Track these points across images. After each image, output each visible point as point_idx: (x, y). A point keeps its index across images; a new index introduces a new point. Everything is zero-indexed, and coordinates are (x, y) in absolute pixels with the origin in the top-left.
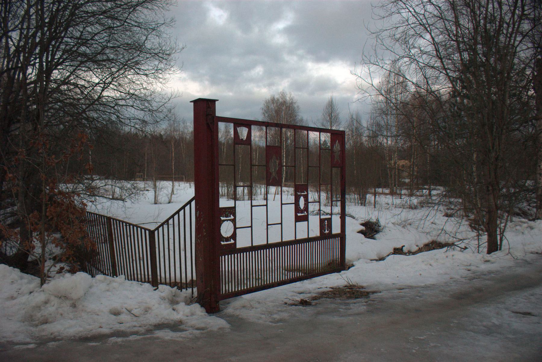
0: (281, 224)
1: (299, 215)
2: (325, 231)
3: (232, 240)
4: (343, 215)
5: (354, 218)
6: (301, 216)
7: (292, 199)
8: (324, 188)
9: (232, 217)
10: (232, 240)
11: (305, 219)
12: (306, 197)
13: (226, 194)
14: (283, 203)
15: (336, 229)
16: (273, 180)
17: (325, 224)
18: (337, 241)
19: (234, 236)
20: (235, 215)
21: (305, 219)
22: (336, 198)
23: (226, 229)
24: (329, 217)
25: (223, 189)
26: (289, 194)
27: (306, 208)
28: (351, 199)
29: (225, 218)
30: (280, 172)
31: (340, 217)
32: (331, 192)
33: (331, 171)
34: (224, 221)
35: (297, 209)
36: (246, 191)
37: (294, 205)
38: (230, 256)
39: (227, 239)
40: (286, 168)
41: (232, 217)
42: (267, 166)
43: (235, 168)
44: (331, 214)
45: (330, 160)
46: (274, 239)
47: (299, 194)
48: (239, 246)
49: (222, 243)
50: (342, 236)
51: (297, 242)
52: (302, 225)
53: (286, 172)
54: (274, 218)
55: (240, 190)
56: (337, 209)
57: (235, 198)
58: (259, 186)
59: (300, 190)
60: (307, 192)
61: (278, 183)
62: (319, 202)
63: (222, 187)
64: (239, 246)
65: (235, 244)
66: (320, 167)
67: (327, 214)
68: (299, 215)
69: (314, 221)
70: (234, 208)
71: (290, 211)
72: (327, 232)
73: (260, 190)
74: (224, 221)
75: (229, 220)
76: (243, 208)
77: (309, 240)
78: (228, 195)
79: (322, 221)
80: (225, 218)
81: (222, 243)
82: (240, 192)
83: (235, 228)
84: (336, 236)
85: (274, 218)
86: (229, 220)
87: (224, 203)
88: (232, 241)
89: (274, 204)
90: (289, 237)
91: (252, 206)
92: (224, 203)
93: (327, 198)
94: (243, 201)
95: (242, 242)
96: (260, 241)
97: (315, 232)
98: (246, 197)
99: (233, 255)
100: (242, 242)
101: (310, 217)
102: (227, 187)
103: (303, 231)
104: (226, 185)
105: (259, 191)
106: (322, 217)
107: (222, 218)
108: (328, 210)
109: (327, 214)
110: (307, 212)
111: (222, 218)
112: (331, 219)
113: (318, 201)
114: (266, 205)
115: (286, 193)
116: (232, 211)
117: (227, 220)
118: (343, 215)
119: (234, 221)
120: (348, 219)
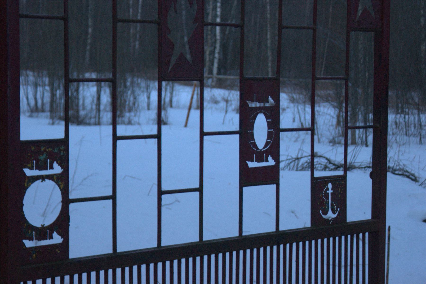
0: (200, 190)
1: (252, 165)
2: (326, 213)
3: (55, 235)
4: (379, 171)
5: (415, 180)
6: (258, 169)
7: (233, 121)
8: (44, 94)
9: (57, 169)
10: (55, 235)
11: (271, 176)
12: (273, 116)
13: (47, 107)
14: (206, 130)
15: (358, 208)
16: (180, 66)
17: (327, 192)
18: (362, 244)
19: (62, 224)
20: (64, 163)
21: (271, 176)
22: (365, 120)
23: (39, 203)
24: (340, 173)
25: (32, 91)
26: (230, 109)
27: (273, 148)
28: (407, 125)
29: (36, 173)
30: (197, 41)
31: (371, 175)
32: (345, 104)
33: (348, 39)
34: (34, 179)
35: (247, 150)
36: (106, 98)
37: (237, 136)
38: (152, 266)
39: (43, 233)
40: (223, 32)
41: (57, 169)
42: (162, 26)
43: (242, 34)
44: (347, 167)
45: (346, 5)
46: (180, 231)
47: (252, 105)
48: (75, 253)
49: (28, 244)
50: (376, 229)
51: (243, 243)
52: (260, 196)
53: (224, 46)
54: (180, 171)
55: (88, 93)
56: (364, 155)
57: (69, 114)
58: (143, 84)
59: (257, 96)
60: (277, 100)
61: (190, 72)
62: (312, 130)
63: (36, 85)
64: (75, 253)
65: (65, 246)
66: (314, 30)
67: (337, 167)
68: (252, 165)
69: (296, 187)
70: (64, 143)
71: (225, 154)
72: (331, 215)
73: (145, 96)
74: (34, 179)
75: (50, 177)
76: (88, 145)
77: (279, 238)
78: (52, 110)
79: (317, 185)
80: (36, 173)
81: (28, 244)
82: (88, 101)
83: (66, 201)
84: (359, 227)
85: (180, 171)
86: (50, 177)
87: (34, 128)
88: (57, 239)
89: (180, 137)
90: (221, 227)
91: (116, 138)
92: (34, 128)
93: (338, 123)
94: (97, 128)
95: (87, 239)
96: (137, 237)
97: (298, 215)
98: (107, 116)
99: (160, 265)
100: (87, 239)
101: (285, 176)
102: (51, 84)
103: (260, 211)
104: (47, 80)
105: (142, 99)
106: (317, 174)
107: (28, 172)
108: (337, 155)
109: (337, 167)
110: (277, 158)
111: (28, 172)
112: (344, 178)
113: (310, 129)
114: (158, 137)
115: (223, 104)
116: (57, 151)
117: (43, 178)
118: (379, 171)
119: (63, 181)
120: (393, 182)
